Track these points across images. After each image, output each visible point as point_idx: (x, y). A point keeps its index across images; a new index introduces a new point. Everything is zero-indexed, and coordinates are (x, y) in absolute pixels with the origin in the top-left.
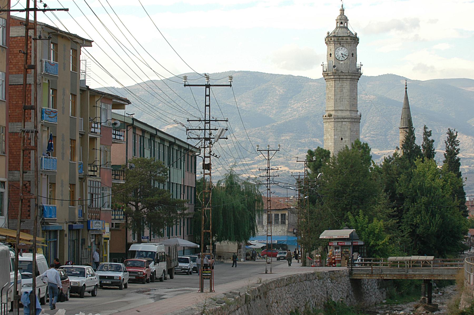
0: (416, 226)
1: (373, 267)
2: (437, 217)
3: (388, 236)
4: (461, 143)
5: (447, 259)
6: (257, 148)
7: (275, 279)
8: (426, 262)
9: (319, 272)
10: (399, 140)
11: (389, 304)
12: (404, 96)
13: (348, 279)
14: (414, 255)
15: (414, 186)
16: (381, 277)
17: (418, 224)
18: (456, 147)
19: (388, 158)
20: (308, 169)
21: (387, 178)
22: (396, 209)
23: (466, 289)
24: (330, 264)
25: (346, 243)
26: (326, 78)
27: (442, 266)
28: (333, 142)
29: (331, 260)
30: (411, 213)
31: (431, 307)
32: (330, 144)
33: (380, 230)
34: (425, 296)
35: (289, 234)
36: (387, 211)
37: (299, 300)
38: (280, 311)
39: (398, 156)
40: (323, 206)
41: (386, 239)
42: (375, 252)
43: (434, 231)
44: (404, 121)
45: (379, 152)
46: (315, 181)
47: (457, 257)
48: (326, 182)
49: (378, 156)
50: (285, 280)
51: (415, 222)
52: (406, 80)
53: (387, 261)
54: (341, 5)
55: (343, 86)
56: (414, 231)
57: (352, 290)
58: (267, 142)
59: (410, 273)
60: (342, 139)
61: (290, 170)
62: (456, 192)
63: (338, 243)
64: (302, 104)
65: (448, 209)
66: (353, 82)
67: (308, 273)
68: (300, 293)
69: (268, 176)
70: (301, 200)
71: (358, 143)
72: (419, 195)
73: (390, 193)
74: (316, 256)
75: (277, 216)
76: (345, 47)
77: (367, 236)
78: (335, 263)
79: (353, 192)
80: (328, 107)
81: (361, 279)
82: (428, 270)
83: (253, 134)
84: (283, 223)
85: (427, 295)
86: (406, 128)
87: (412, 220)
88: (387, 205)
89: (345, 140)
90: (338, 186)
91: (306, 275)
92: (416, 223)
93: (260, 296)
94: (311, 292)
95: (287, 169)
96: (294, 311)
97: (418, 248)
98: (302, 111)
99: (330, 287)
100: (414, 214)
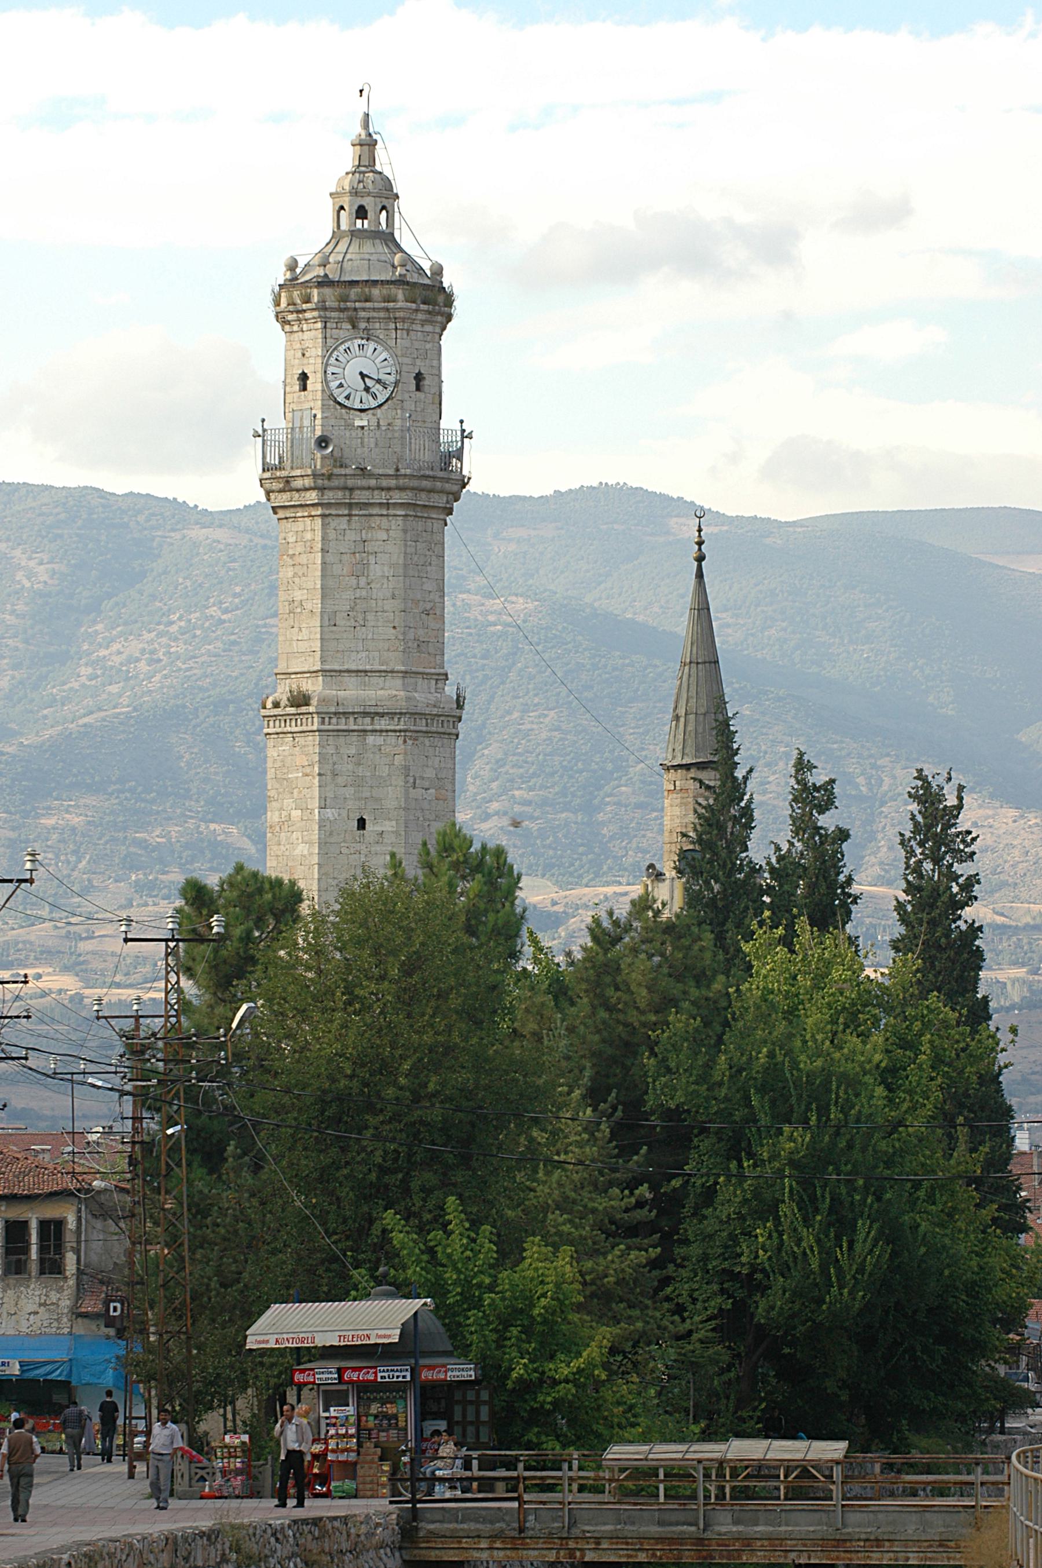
1: (526, 1497)
3: (604, 1335)
5: (915, 1455)
9: (241, 1527)
10: (661, 831)
12: (689, 598)
14: (740, 1435)
15: (740, 1071)
16: (571, 1552)
17: (763, 1271)
19: (606, 924)
21: (599, 1031)
22: (644, 1191)
25: (385, 1374)
26: (282, 499)
27: (892, 1495)
28: (315, 837)
30: (725, 1211)
32: (302, 849)
33: (561, 1303)
35: (81, 1328)
36: (601, 1203)
40: (264, 1175)
41: (592, 1353)
42: (539, 1417)
44: (691, 727)
46: (222, 1046)
47: (968, 1448)
48: (279, 1049)
49: (549, 915)
51: (744, 1259)
52: (700, 513)
53: (599, 1467)
55: (369, 548)
56: (741, 1310)
60: (362, 824)
61: (87, 992)
62: (961, 1105)
63: (340, 1371)
64: (151, 642)
65: (921, 1193)
66: (420, 525)
67: (183, 1529)
70: (148, 1147)
71: (456, 843)
72: (764, 1120)
74: (227, 1438)
77: (495, 1336)
79: (417, 1099)
81: (462, 1562)
82: (817, 1515)
84: (52, 1267)
86: (701, 766)
88: (601, 1174)
89: (379, 829)
90: (340, 1070)
92: (754, 1268)
95: (69, 983)
100: (742, 1218)
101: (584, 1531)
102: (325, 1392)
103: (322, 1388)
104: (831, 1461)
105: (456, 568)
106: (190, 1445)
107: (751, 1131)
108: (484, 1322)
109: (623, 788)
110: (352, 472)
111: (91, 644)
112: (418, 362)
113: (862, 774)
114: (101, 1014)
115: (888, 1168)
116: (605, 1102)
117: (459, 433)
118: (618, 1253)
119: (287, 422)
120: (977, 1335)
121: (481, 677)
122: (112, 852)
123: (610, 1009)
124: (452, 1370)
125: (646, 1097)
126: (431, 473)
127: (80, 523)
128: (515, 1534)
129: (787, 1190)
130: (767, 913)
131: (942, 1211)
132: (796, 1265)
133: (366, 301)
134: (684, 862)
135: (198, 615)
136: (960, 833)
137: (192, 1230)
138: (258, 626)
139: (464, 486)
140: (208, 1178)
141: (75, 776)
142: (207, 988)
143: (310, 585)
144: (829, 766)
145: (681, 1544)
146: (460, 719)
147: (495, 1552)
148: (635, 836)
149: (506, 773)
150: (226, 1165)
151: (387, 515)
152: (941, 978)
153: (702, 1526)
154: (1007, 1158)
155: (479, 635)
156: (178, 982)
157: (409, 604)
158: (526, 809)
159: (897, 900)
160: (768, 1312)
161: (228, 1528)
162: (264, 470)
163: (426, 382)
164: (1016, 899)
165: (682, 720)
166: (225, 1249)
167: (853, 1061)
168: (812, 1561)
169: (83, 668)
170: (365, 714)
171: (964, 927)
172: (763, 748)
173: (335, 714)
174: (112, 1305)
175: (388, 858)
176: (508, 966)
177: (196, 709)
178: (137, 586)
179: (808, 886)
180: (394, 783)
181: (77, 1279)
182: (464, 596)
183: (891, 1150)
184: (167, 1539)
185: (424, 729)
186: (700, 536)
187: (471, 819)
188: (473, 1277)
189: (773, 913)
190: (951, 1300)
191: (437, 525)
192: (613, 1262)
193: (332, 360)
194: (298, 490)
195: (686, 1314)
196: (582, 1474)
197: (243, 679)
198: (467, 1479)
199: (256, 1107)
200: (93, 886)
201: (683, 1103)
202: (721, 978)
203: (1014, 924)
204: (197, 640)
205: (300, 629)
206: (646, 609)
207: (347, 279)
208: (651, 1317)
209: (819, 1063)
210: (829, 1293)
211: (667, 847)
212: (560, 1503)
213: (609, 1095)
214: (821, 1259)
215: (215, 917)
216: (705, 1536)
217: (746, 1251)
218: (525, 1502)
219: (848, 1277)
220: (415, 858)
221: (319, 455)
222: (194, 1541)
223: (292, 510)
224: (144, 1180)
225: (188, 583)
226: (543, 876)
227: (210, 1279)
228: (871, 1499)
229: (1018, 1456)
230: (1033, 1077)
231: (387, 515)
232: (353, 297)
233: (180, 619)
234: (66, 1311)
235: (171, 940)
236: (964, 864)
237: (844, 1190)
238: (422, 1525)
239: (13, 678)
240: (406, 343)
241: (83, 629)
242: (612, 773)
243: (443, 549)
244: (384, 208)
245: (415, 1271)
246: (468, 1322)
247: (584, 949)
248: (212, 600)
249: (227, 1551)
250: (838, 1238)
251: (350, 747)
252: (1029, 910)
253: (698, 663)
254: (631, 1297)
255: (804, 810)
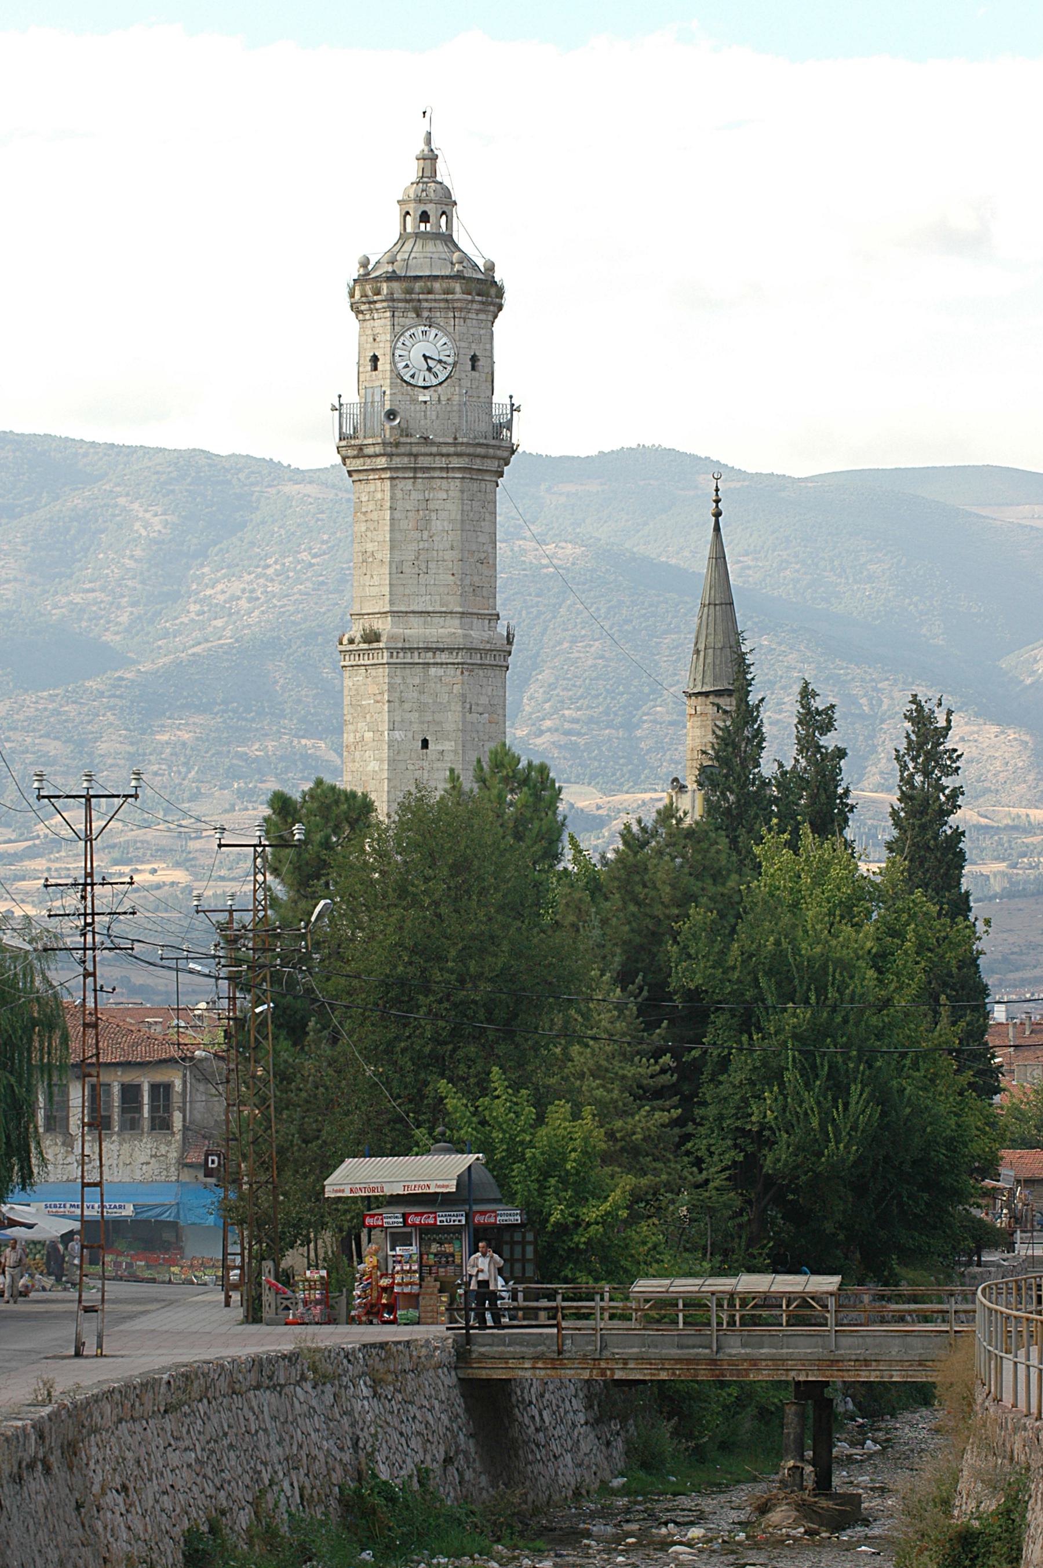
0: (763, 1138)
2: (853, 1100)
3: (627, 1182)
4: (969, 762)
5: (905, 1288)
6: (36, 785)
7: (118, 1381)
8: (804, 1299)
9: (317, 1350)
11: (637, 1493)
13: (451, 1380)
14: (751, 1270)
15: (750, 957)
17: (771, 1128)
18: (944, 781)
19: (635, 828)
20: (269, 878)
22: (666, 1059)
23: (984, 1426)
24: (367, 1313)
25: (443, 1218)
27: (883, 1321)
29: (375, 1294)
30: (738, 1077)
31: (828, 1509)
32: (374, 766)
34: (802, 1458)
35: (186, 1176)
36: (630, 1071)
37: (226, 1475)
38: (138, 1526)
39: (680, 821)
40: (338, 1048)
43: (843, 1161)
44: (709, 660)
45: (601, 800)
46: (303, 937)
49: (595, 817)
50: (163, 1389)
51: (754, 1119)
52: (718, 471)
53: (627, 1299)
54: (423, 135)
55: (431, 506)
56: (752, 1162)
57: (472, 1431)
58: (91, 754)
59: (734, 1351)
60: (425, 744)
61: (196, 884)
62: (945, 984)
63: (405, 1216)
64: (251, 583)
65: (908, 1062)
66: (475, 486)
68: (231, 1446)
69: (85, 915)
71: (506, 760)
73: (641, 989)
75: (131, 1093)
76: (439, 327)
77: (536, 1186)
78: (391, 1308)
80: (363, 599)
81: (509, 1380)
82: (814, 1339)
83: (28, 718)
84: (161, 1124)
85: (809, 1454)
86: (718, 693)
87: (742, 1112)
89: (440, 748)
91: (257, 1363)
92: (763, 1127)
93: (44, 1462)
94: (279, 1443)
95: (180, 876)
96: (205, 1528)
97: (770, 1239)
98: (249, 613)
99: (369, 1418)
101: (613, 1353)
102: (392, 1234)
103: (389, 1230)
104: (827, 1293)
105: (513, 519)
106: (277, 1278)
107: (759, 1010)
108: (526, 1173)
109: (658, 709)
110: (416, 441)
111: (198, 584)
112: (474, 346)
113: (865, 696)
114: (200, 908)
115: (879, 1040)
116: (633, 983)
117: (509, 407)
118: (644, 1113)
119: (361, 398)
120: (955, 1184)
121: (535, 613)
122: (217, 764)
123: (638, 903)
124: (501, 1215)
125: (669, 980)
126: (485, 441)
127: (189, 480)
128: (555, 1356)
129: (790, 1059)
130: (775, 821)
131: (925, 1077)
132: (798, 1121)
133: (429, 293)
134: (703, 776)
135: (291, 559)
136: (948, 751)
137: (278, 1094)
138: (343, 569)
139: (513, 452)
140: (293, 1049)
141: (186, 698)
142: (291, 886)
143: (380, 538)
144: (836, 689)
145: (698, 1365)
146: (510, 653)
147: (538, 1371)
148: (669, 749)
149: (557, 695)
150: (308, 1038)
151: (447, 478)
152: (928, 875)
153: (715, 1349)
154: (984, 1029)
155: (534, 576)
156: (264, 882)
157: (466, 554)
158: (575, 726)
159: (892, 807)
160: (775, 1164)
161: (306, 1351)
162: (340, 439)
163: (480, 363)
164: (998, 803)
165: (702, 653)
166: (308, 1110)
167: (848, 948)
168: (810, 1379)
169: (192, 605)
170: (428, 649)
171: (949, 832)
172: (780, 673)
173: (402, 649)
174: (210, 1158)
175: (448, 773)
176: (552, 866)
177: (290, 640)
178: (239, 534)
179: (810, 797)
180: (453, 708)
181: (184, 1134)
182: (521, 542)
183: (881, 1025)
184: (254, 1361)
185: (479, 662)
186: (717, 495)
187: (527, 735)
188: (517, 1136)
189: (780, 820)
190: (933, 1153)
191: (490, 486)
192: (640, 1121)
193: (399, 345)
194: (369, 456)
195: (704, 1166)
196: (612, 1304)
197: (329, 614)
198: (515, 1308)
199: (330, 989)
200: (201, 793)
201: (702, 985)
202: (735, 877)
203: (996, 825)
204: (290, 581)
205: (372, 576)
206: (678, 553)
207: (412, 274)
208: (674, 1169)
209: (818, 949)
210: (827, 1147)
211: (689, 763)
212: (593, 1329)
213: (637, 977)
214: (820, 1119)
215: (297, 826)
216: (718, 1357)
217: (756, 1112)
218: (563, 1329)
219: (844, 1134)
220: (471, 773)
221: (387, 426)
222: (277, 1362)
223: (365, 473)
224: (237, 1051)
225: (283, 532)
226: (589, 784)
227: (293, 1135)
228: (861, 1325)
229: (984, 1289)
230: (1012, 957)
231: (447, 478)
232: (417, 290)
233: (276, 563)
234: (174, 1161)
235: (260, 845)
236: (950, 778)
237: (840, 1059)
238: (474, 1348)
239: (132, 613)
240: (464, 329)
241: (192, 572)
242: (648, 695)
243: (495, 507)
244: (444, 213)
245: (467, 1132)
246: (513, 1174)
247: (616, 851)
248: (303, 547)
249: (306, 1371)
250: (835, 1100)
251: (415, 678)
252: (1009, 813)
253: (715, 605)
254: (655, 1151)
255: (807, 731)
